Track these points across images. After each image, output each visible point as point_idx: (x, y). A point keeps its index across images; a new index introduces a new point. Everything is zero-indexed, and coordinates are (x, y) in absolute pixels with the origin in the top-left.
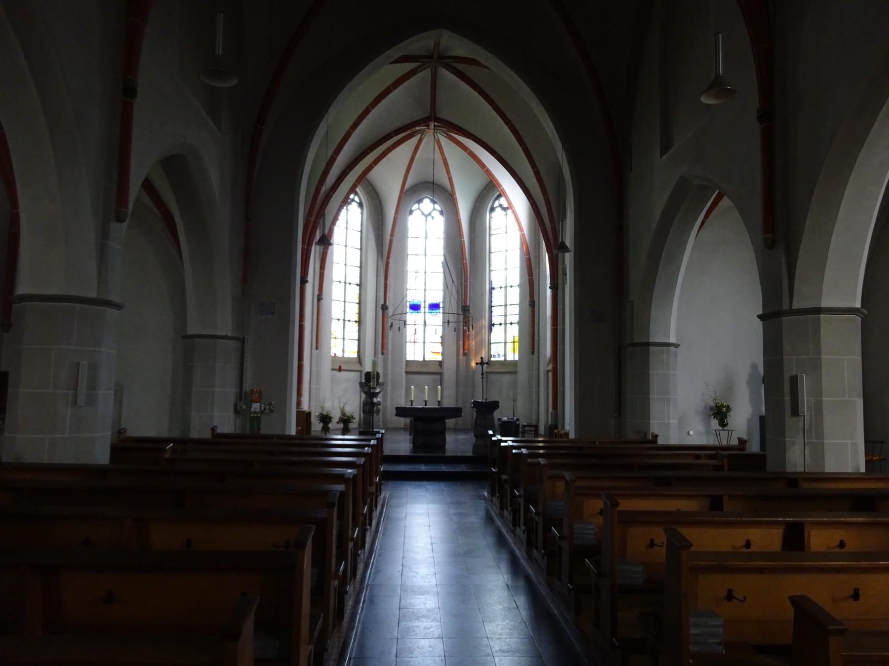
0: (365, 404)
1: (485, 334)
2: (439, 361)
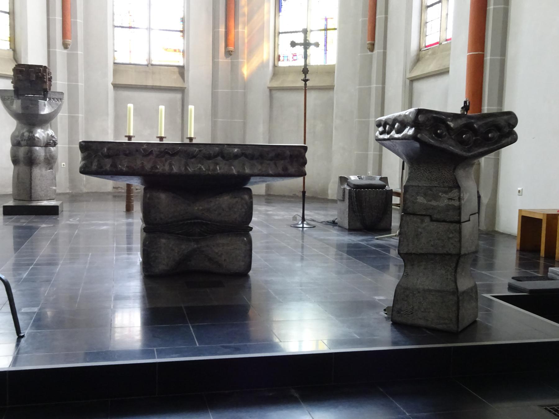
0: (16, 144)
1: (269, 12)
2: (178, 67)
